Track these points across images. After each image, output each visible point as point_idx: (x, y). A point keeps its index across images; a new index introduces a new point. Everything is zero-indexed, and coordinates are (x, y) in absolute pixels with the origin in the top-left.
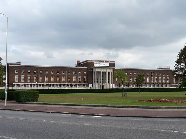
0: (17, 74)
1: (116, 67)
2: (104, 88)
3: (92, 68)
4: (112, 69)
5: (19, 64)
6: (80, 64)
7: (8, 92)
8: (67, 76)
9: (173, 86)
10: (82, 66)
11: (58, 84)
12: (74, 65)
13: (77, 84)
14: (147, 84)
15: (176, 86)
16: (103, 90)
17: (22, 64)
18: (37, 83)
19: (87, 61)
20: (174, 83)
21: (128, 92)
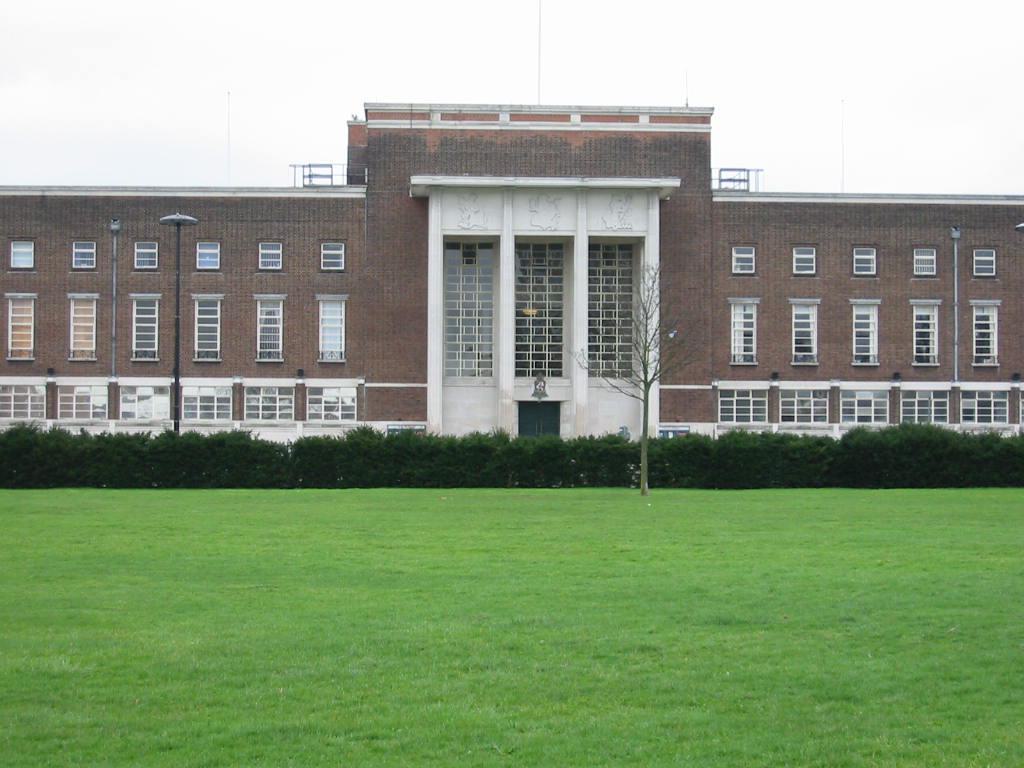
2: (568, 431)
4: (639, 202)
8: (127, 287)
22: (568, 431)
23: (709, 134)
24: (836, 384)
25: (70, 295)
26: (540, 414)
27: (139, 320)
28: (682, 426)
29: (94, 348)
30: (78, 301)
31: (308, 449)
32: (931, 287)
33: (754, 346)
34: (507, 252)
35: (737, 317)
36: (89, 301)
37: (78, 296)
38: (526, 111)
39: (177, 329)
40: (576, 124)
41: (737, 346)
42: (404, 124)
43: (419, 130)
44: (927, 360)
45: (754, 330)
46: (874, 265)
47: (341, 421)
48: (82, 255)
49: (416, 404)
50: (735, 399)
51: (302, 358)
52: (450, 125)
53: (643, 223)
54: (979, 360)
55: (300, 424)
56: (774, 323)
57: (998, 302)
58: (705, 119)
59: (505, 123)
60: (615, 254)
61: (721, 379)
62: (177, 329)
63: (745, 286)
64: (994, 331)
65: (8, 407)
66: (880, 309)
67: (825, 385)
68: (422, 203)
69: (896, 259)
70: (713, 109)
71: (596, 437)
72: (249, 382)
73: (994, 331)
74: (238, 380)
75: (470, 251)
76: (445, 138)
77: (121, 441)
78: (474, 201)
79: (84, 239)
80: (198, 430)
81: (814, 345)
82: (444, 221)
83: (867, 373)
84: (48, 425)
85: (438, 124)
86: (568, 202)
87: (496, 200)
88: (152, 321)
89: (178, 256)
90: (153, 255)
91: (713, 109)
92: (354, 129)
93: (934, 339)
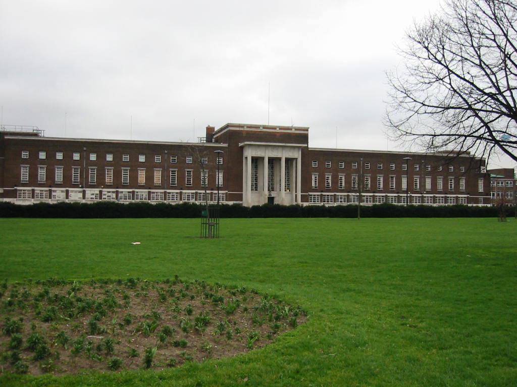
0: (25, 161)
1: (314, 143)
2: (276, 202)
3: (242, 148)
4: (297, 149)
5: (36, 135)
6: (214, 135)
7: (357, 211)
8: (169, 167)
9: (477, 201)
10: (217, 141)
11: (451, 196)
12: (196, 136)
13: (165, 192)
14: (401, 195)
15: (486, 201)
16: (271, 210)
17: (52, 131)
18: (82, 187)
19: (228, 126)
20: (481, 194)
21: (221, 217)
22: (276, 202)
23: (308, 134)
24: (197, 191)
25: (138, 168)
26: (271, 199)
27: (175, 176)
28: (485, 205)
29: (160, 182)
30: (156, 170)
31: (339, 208)
32: (357, 171)
33: (317, 184)
34: (266, 161)
35: (313, 177)
36: (159, 170)
37: (157, 169)
38: (269, 127)
39: (181, 178)
40: (278, 130)
41: (313, 184)
42: (238, 129)
43: (241, 131)
44: (355, 188)
45: (317, 180)
46: (222, 162)
47: (128, 200)
48: (158, 159)
49: (240, 197)
50: (202, 195)
51: (213, 186)
52: (248, 129)
53: (297, 155)
54: (366, 188)
55: (33, 200)
56: (322, 179)
57: (370, 175)
58: (307, 130)
59: (261, 129)
60: (289, 161)
61: (310, 192)
62: (181, 178)
63: (315, 170)
64: (343, 181)
65: (203, 196)
66: (345, 176)
67: (333, 194)
68: (242, 148)
69: (348, 165)
70: (309, 128)
71: (261, 206)
72: (168, 191)
73: (343, 181)
74: (33, 188)
75: (256, 161)
76: (248, 132)
77: (137, 204)
78: (272, 151)
79: (158, 154)
80: (171, 203)
81: (330, 184)
82: (249, 153)
83: (440, 193)
84: (181, 202)
85: (246, 129)
86: (280, 149)
87: (264, 148)
88: (78, 173)
89: (101, 157)
90: (27, 155)
91: (309, 128)
92: (207, 128)
93: (418, 185)
